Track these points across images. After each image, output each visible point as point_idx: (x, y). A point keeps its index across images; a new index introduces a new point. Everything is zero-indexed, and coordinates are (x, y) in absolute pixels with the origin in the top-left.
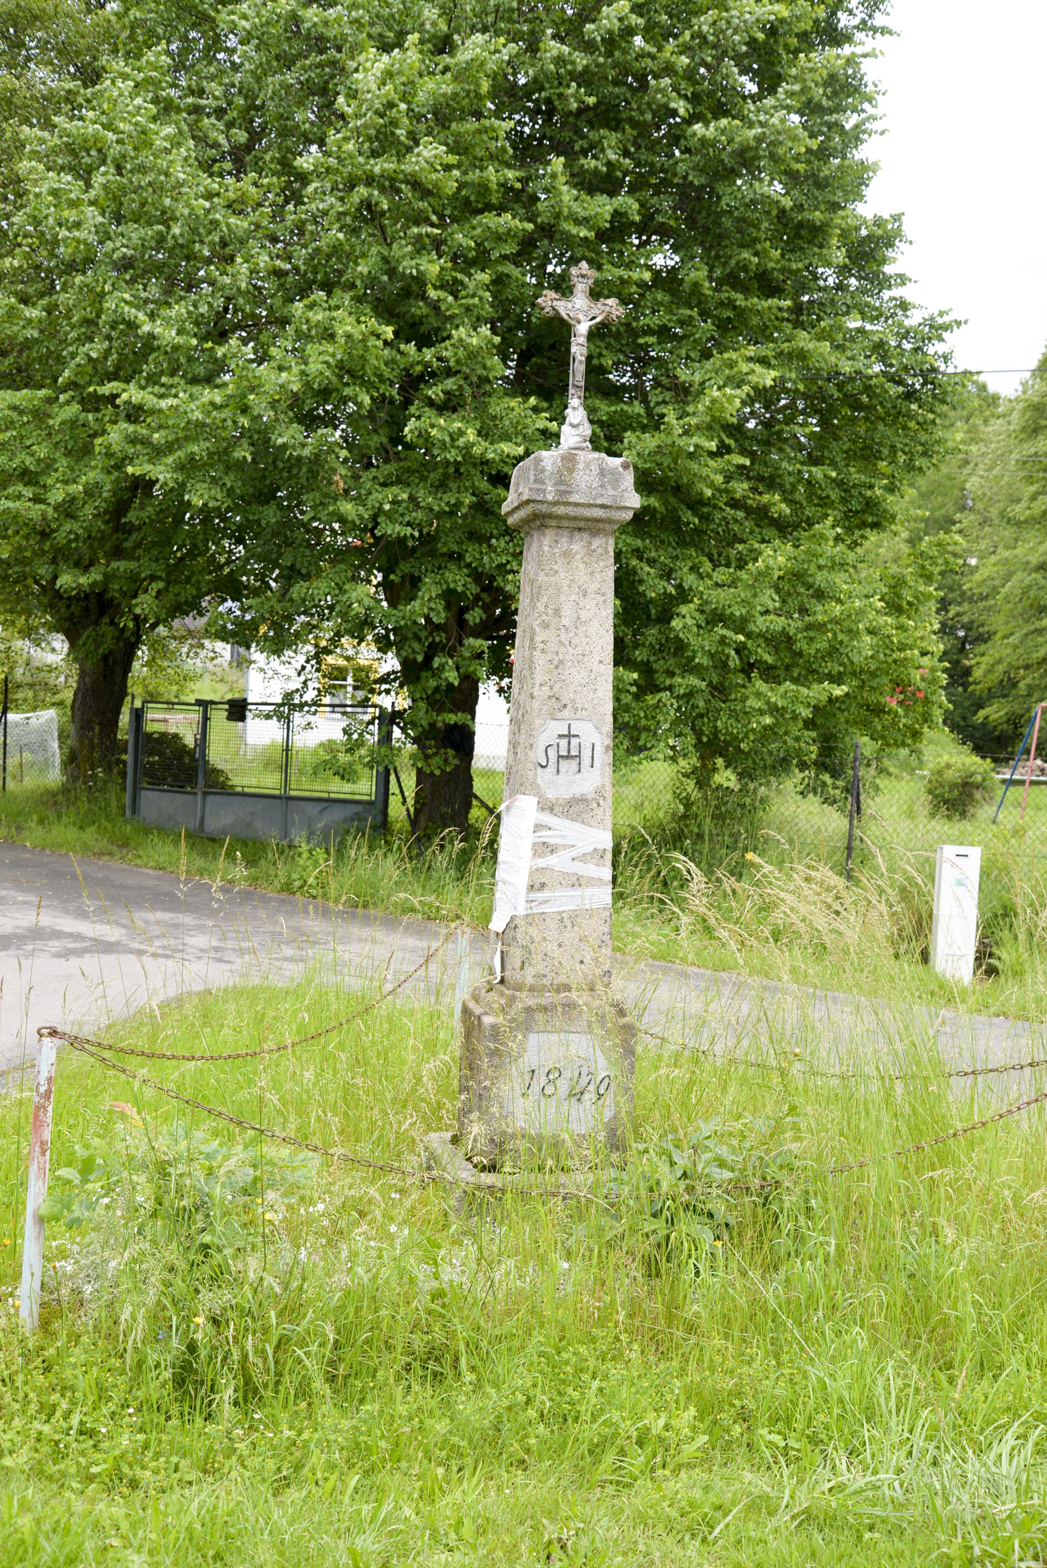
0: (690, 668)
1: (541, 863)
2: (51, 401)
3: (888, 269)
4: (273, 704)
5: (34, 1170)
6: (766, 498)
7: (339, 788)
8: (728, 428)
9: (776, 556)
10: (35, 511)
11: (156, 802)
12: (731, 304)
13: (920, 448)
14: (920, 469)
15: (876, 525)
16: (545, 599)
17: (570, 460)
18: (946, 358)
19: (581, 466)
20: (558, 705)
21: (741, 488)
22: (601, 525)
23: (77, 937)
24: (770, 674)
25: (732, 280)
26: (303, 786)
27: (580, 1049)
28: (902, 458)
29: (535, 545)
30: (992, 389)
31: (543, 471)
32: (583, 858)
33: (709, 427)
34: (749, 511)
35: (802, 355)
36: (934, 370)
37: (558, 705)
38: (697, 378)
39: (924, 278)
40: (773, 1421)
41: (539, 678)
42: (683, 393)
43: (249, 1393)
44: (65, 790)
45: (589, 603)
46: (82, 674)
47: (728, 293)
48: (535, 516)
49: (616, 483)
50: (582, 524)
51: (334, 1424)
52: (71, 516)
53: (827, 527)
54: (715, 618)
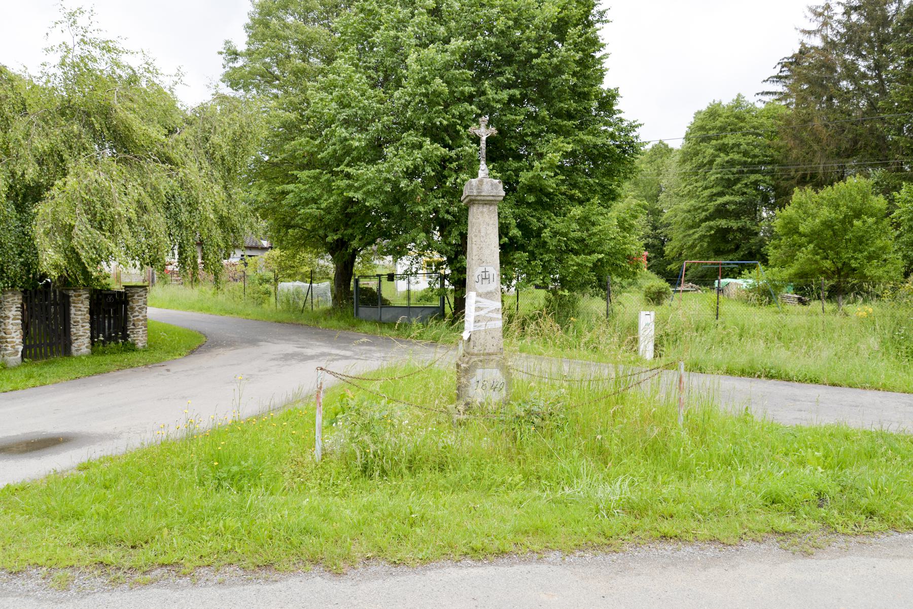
0: (548, 251)
1: (478, 313)
2: (321, 173)
3: (615, 108)
4: (406, 276)
5: (317, 411)
6: (573, 192)
7: (428, 304)
8: (558, 167)
9: (577, 211)
10: (317, 213)
11: (364, 311)
12: (557, 124)
15: (614, 199)
17: (481, 181)
20: (481, 262)
21: (563, 188)
23: (337, 355)
24: (576, 253)
25: (558, 114)
26: (413, 303)
27: (493, 374)
30: (670, 146)
32: (491, 312)
33: (549, 167)
34: (567, 196)
35: (581, 141)
36: (633, 142)
37: (481, 262)
38: (545, 150)
39: (627, 108)
40: (547, 478)
41: (474, 253)
42: (541, 156)
43: (384, 472)
44: (333, 309)
46: (337, 268)
47: (555, 120)
49: (496, 188)
51: (409, 480)
52: (330, 213)
53: (596, 200)
54: (555, 234)
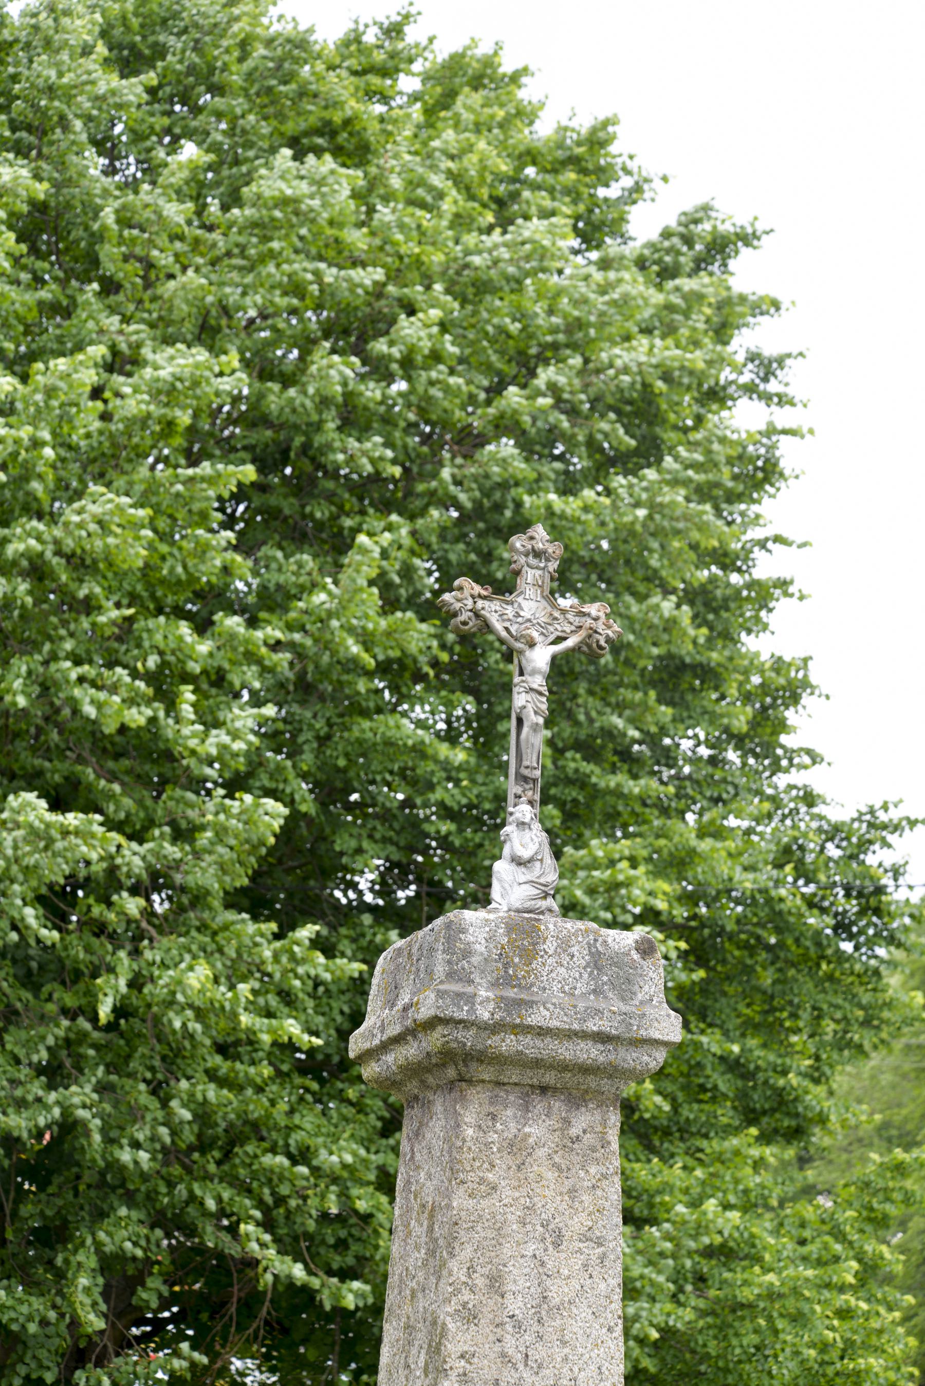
13: (860, 1014)
14: (859, 1047)
16: (466, 1253)
18: (897, 872)
19: (550, 946)
22: (592, 1082)
28: (829, 1027)
29: (436, 1128)
31: (467, 953)
36: (880, 890)
45: (567, 1262)
48: (448, 1056)
49: (625, 986)
50: (550, 1078)
